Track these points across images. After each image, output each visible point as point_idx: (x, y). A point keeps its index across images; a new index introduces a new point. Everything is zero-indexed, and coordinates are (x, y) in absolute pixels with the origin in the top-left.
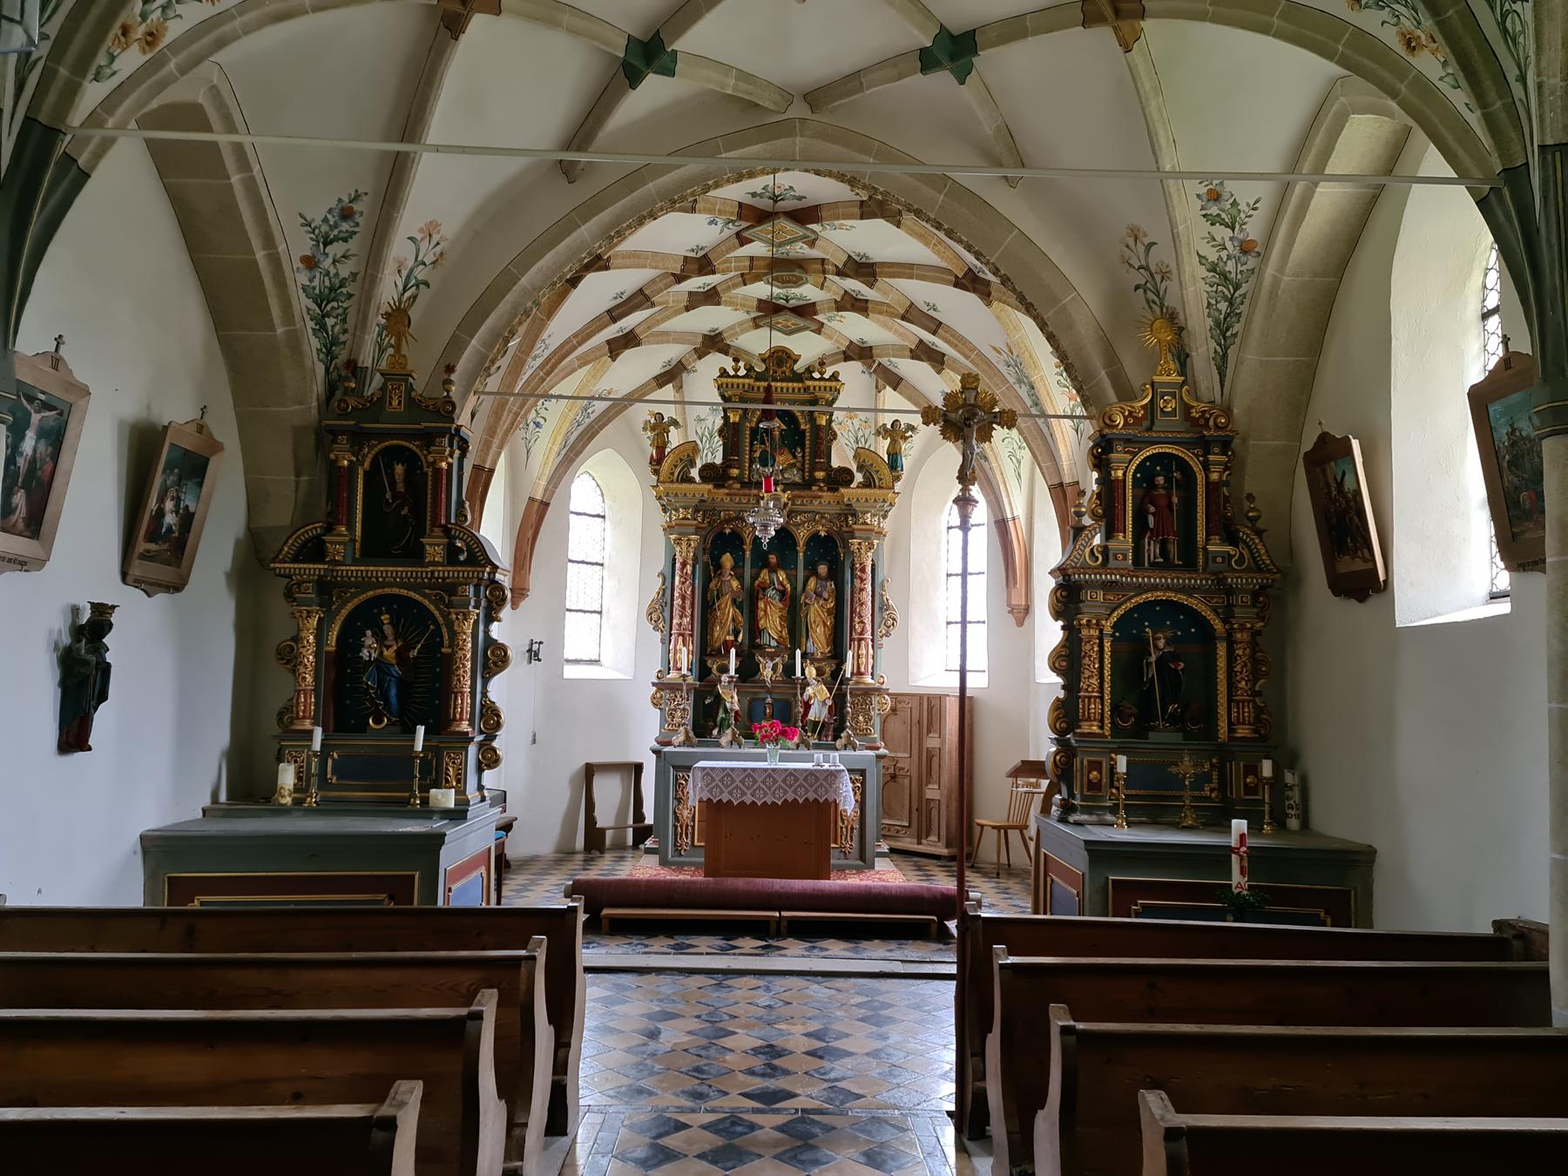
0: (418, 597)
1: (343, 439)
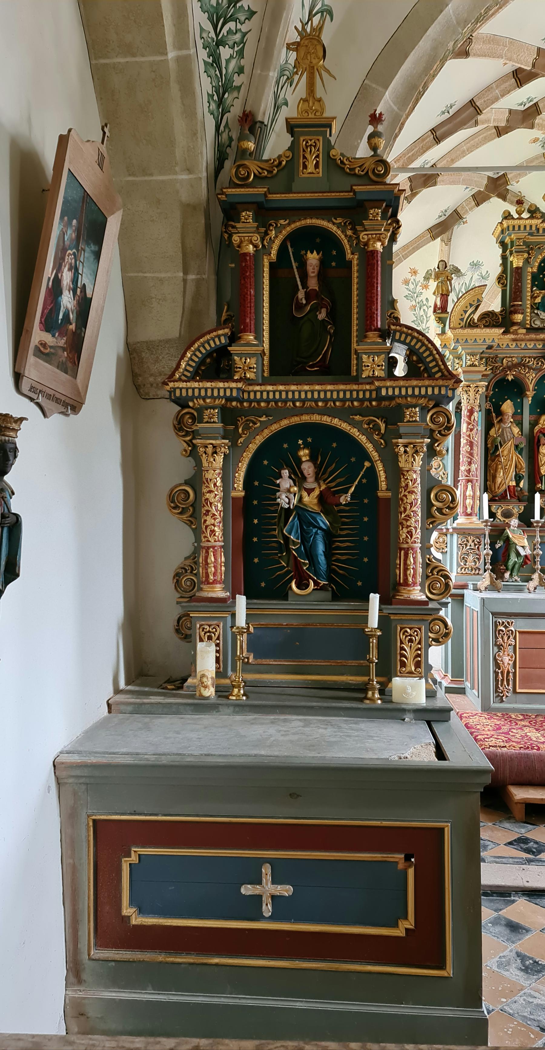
0: (345, 426)
1: (247, 216)
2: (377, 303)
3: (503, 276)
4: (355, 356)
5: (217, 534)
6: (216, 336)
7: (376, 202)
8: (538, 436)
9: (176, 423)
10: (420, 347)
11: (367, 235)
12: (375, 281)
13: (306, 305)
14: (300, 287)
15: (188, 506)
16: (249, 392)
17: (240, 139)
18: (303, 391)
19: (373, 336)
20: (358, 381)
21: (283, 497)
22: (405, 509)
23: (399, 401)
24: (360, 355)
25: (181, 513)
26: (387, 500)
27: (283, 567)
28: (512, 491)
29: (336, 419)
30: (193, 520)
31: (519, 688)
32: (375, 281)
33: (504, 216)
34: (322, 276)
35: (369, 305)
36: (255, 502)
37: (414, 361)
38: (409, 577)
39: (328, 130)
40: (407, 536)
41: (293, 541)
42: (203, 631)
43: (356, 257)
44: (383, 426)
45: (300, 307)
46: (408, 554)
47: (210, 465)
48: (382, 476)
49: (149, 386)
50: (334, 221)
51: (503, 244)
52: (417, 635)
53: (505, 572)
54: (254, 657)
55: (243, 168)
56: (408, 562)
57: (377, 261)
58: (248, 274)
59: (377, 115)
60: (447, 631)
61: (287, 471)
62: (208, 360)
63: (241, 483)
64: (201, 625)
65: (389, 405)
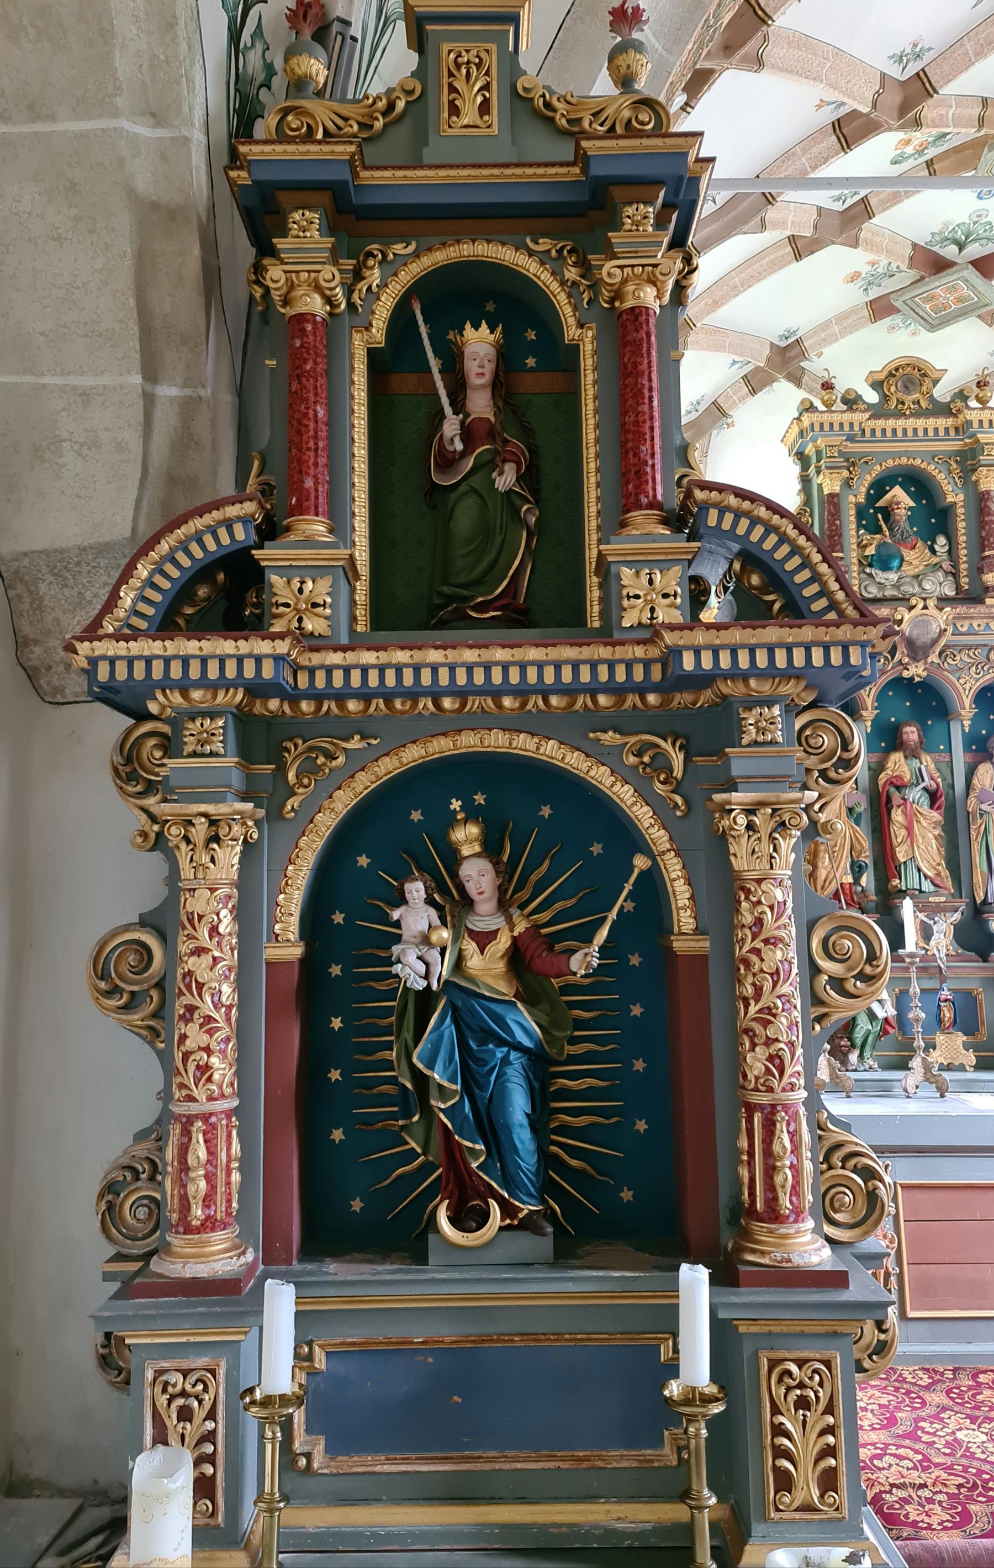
0: (575, 761)
2: (652, 439)
3: (805, 511)
4: (595, 580)
5: (216, 1076)
6: (220, 523)
7: (641, 186)
8: (888, 791)
9: (118, 759)
10: (776, 547)
11: (621, 267)
12: (645, 382)
13: (464, 454)
14: (448, 410)
15: (145, 986)
16: (312, 671)
17: (290, 53)
18: (462, 665)
19: (644, 523)
20: (611, 636)
21: (411, 957)
22: (758, 991)
23: (727, 688)
24: (613, 569)
25: (126, 1008)
26: (700, 960)
27: (413, 1154)
28: (848, 892)
29: (551, 742)
30: (158, 1027)
31: (911, 1309)
32: (645, 382)
33: (802, 408)
34: (501, 385)
35: (630, 444)
36: (336, 970)
37: (755, 588)
38: (780, 1194)
39: (512, 29)
40: (767, 1068)
41: (440, 1087)
42: (164, 1391)
43: (590, 334)
44: (678, 760)
45: (448, 462)
46: (774, 1124)
47: (200, 875)
48: (681, 893)
49: (61, 668)
50: (531, 245)
51: (802, 457)
52: (821, 1384)
53: (849, 1051)
54: (327, 1450)
55: (296, 114)
56: (776, 1148)
57: (648, 335)
58: (308, 367)
59: (630, 11)
60: (882, 1337)
61: (420, 885)
62: (202, 592)
63: (295, 920)
64: (159, 1373)
65: (694, 704)
